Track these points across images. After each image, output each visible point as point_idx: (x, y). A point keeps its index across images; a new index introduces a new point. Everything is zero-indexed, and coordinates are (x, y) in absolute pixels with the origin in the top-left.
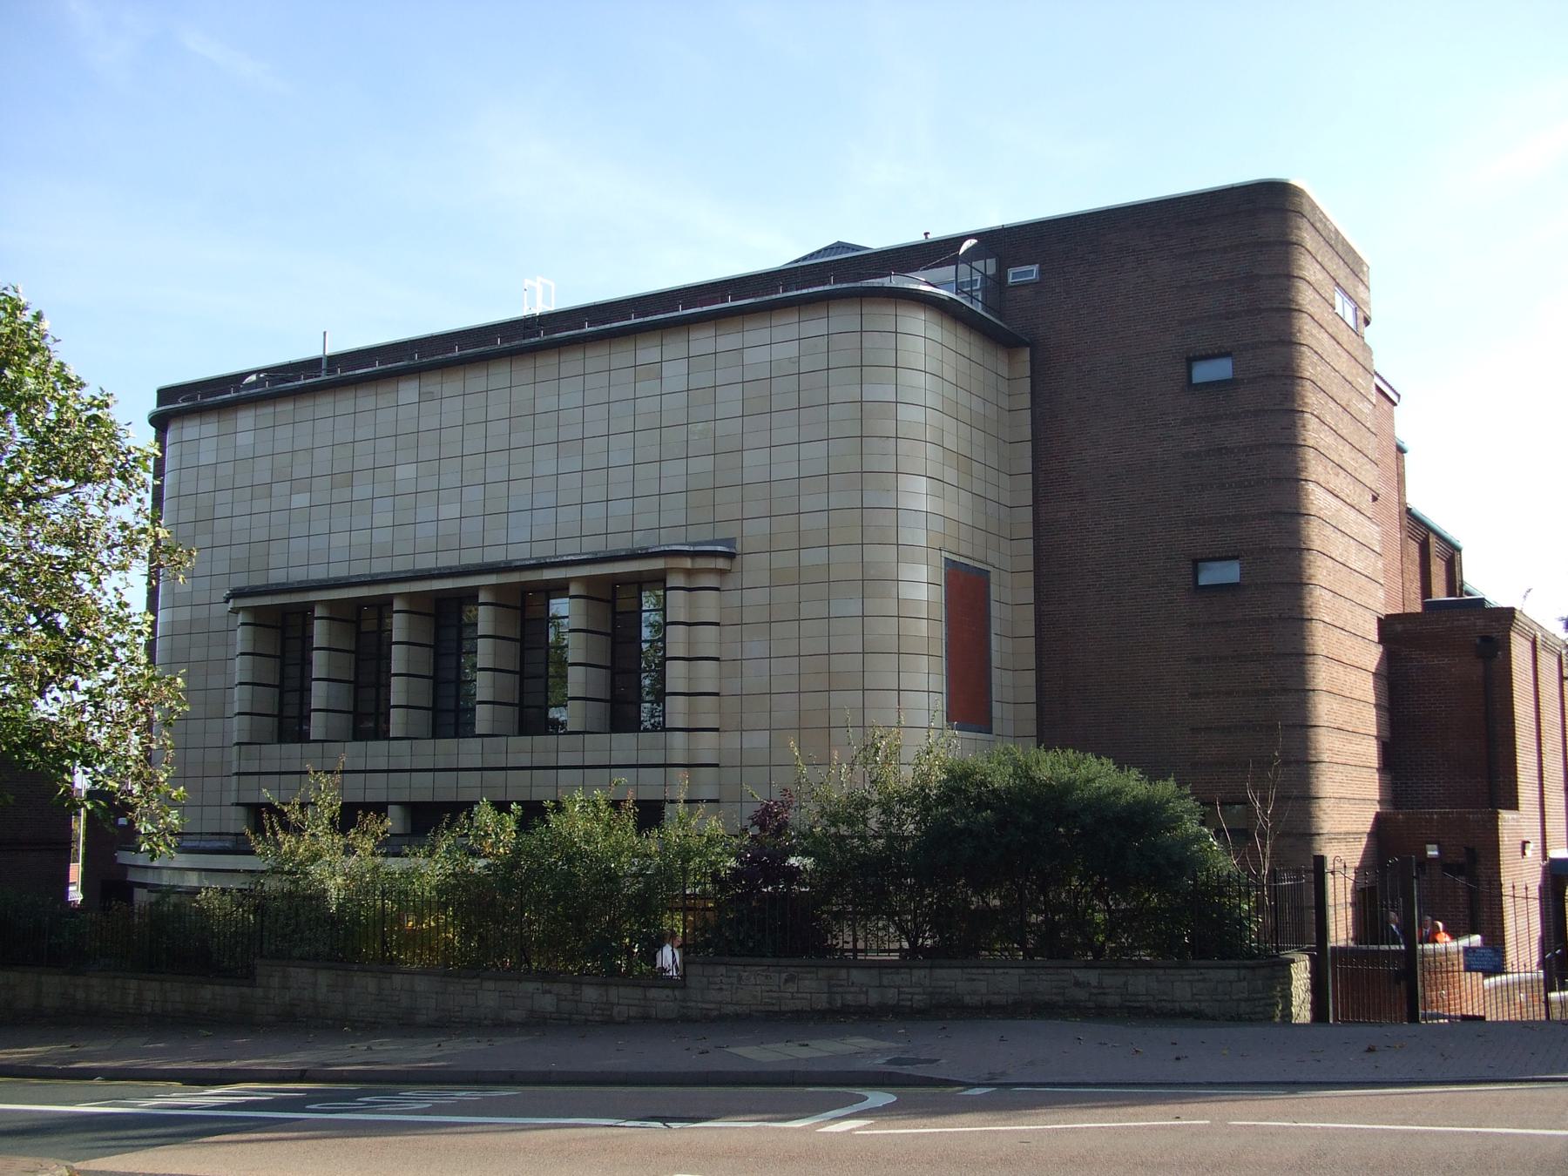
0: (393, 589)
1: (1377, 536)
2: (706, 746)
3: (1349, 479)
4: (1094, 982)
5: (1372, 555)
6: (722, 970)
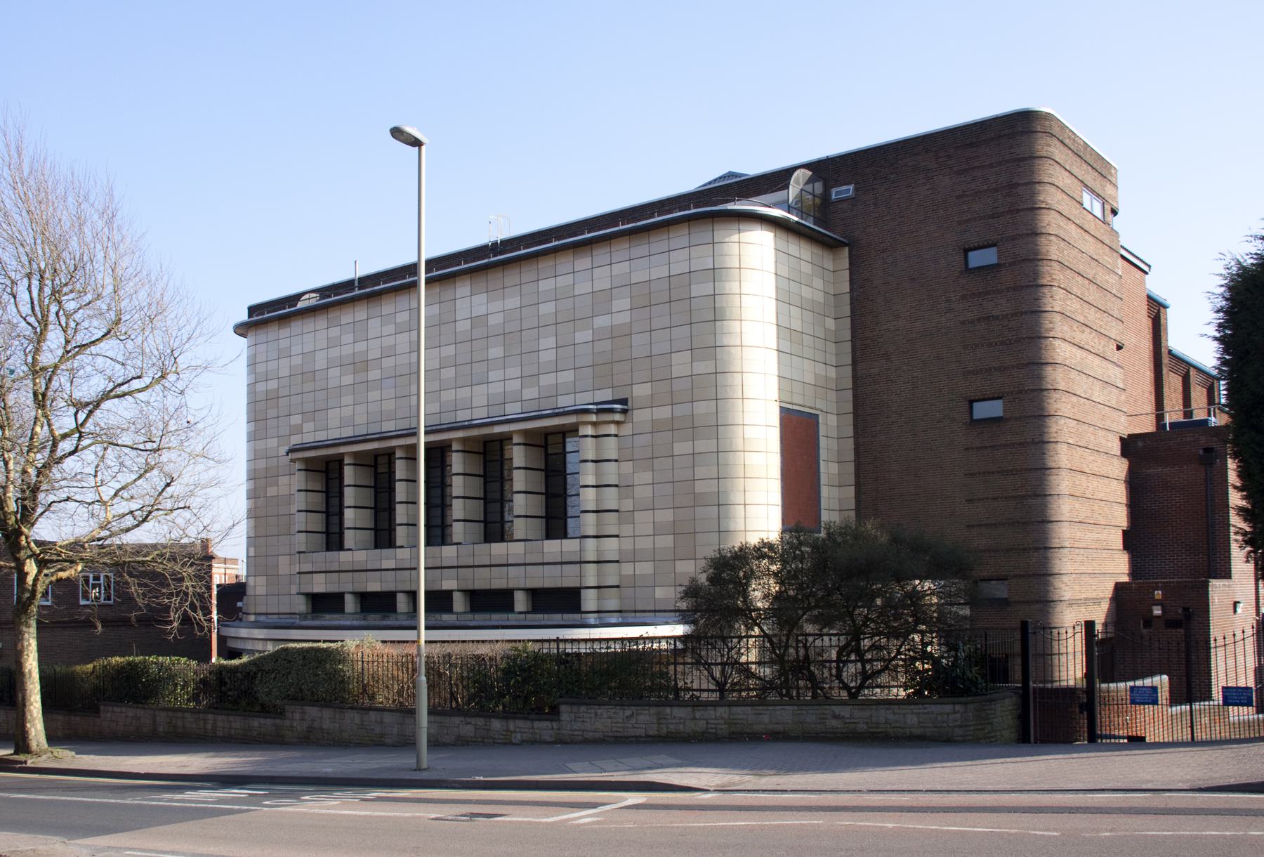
1: (1119, 376)
2: (611, 548)
3: (1094, 334)
4: (847, 715)
5: (1115, 390)
6: (583, 708)
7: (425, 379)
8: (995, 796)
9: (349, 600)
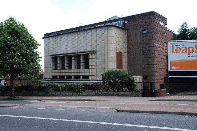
0: (65, 55)
2: (93, 70)
7: (66, 46)
8: (67, 99)
9: (58, 77)
